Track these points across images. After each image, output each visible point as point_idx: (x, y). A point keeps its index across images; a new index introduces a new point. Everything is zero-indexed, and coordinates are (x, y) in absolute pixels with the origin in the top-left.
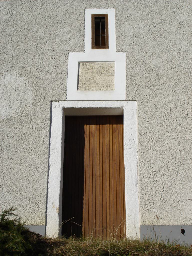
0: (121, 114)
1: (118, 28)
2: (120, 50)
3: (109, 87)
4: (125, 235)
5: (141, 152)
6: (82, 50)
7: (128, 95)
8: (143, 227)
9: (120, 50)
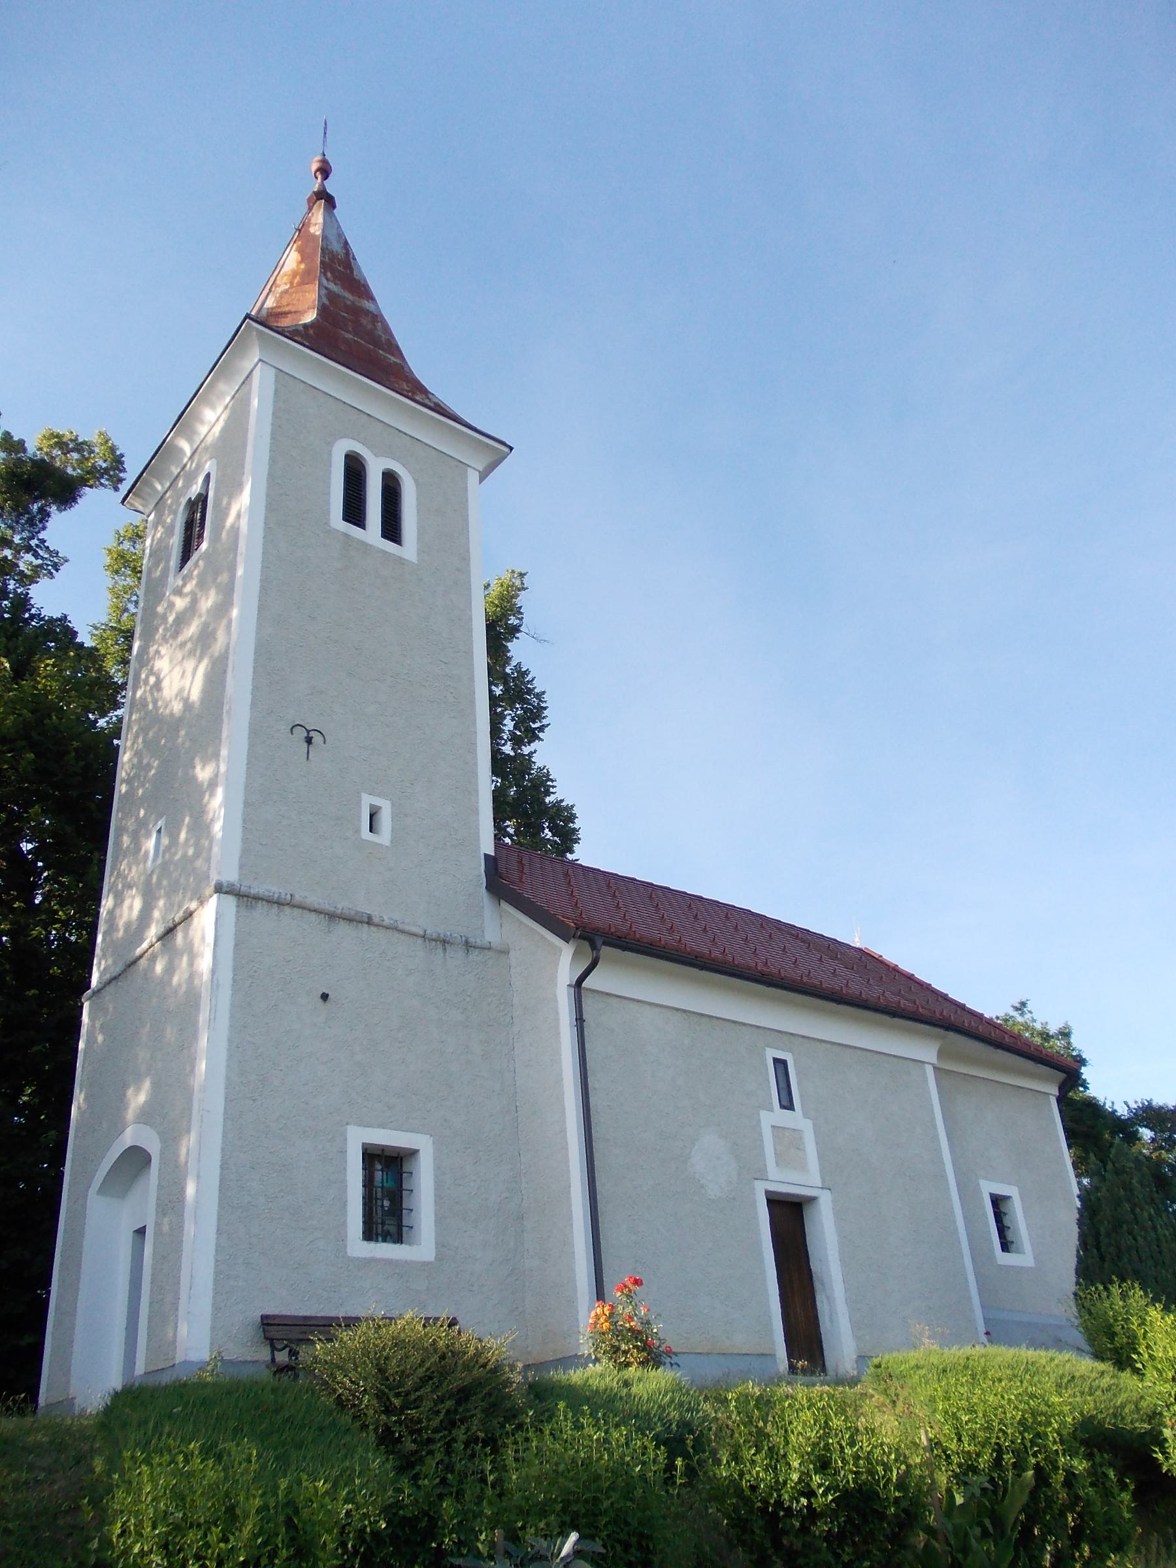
7: (823, 1181)
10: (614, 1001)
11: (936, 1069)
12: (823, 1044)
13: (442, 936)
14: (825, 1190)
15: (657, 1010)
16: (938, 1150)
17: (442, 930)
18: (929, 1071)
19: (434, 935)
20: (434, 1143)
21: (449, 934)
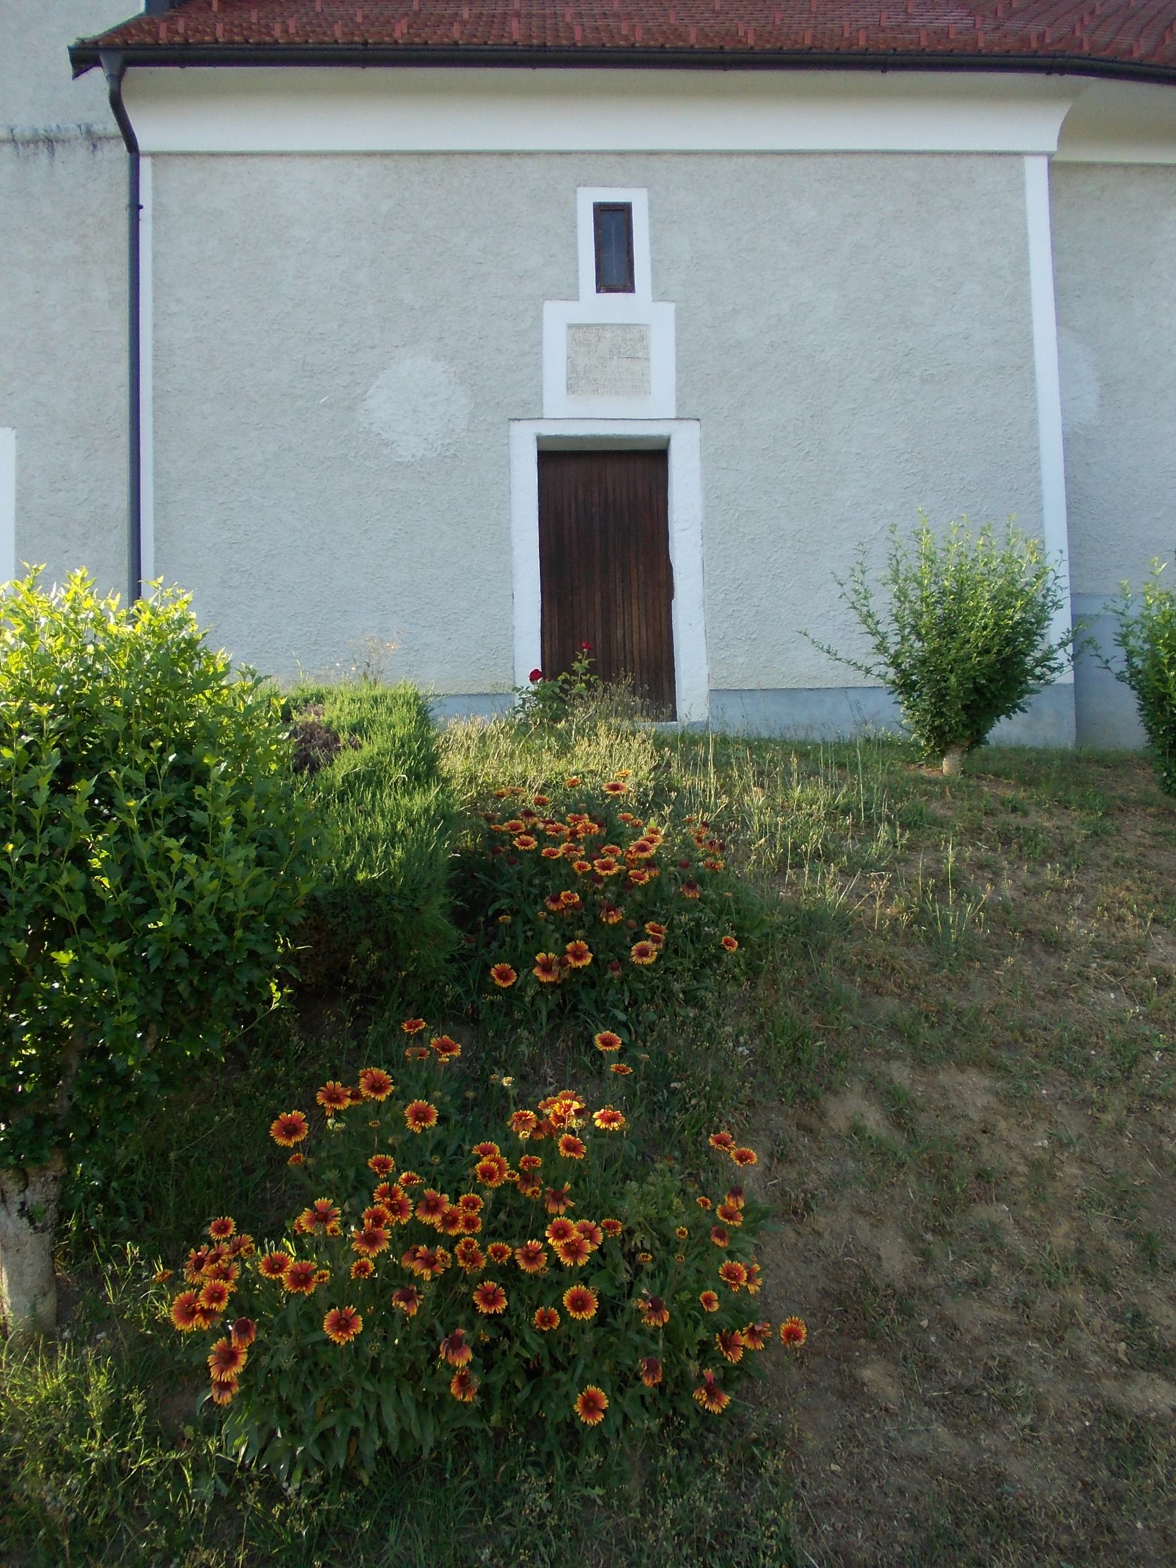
0: (662, 448)
1: (654, 241)
2: (660, 295)
3: (640, 387)
4: (679, 314)
5: (707, 536)
6: (573, 295)
7: (680, 406)
8: (716, 693)
9: (660, 295)
10: (229, 164)
11: (1055, 167)
12: (734, 159)
13: (41, 132)
14: (685, 423)
15: (326, 162)
16: (1024, 319)
17: (43, 123)
18: (1036, 174)
19: (28, 135)
20: (17, 437)
21: (54, 126)
